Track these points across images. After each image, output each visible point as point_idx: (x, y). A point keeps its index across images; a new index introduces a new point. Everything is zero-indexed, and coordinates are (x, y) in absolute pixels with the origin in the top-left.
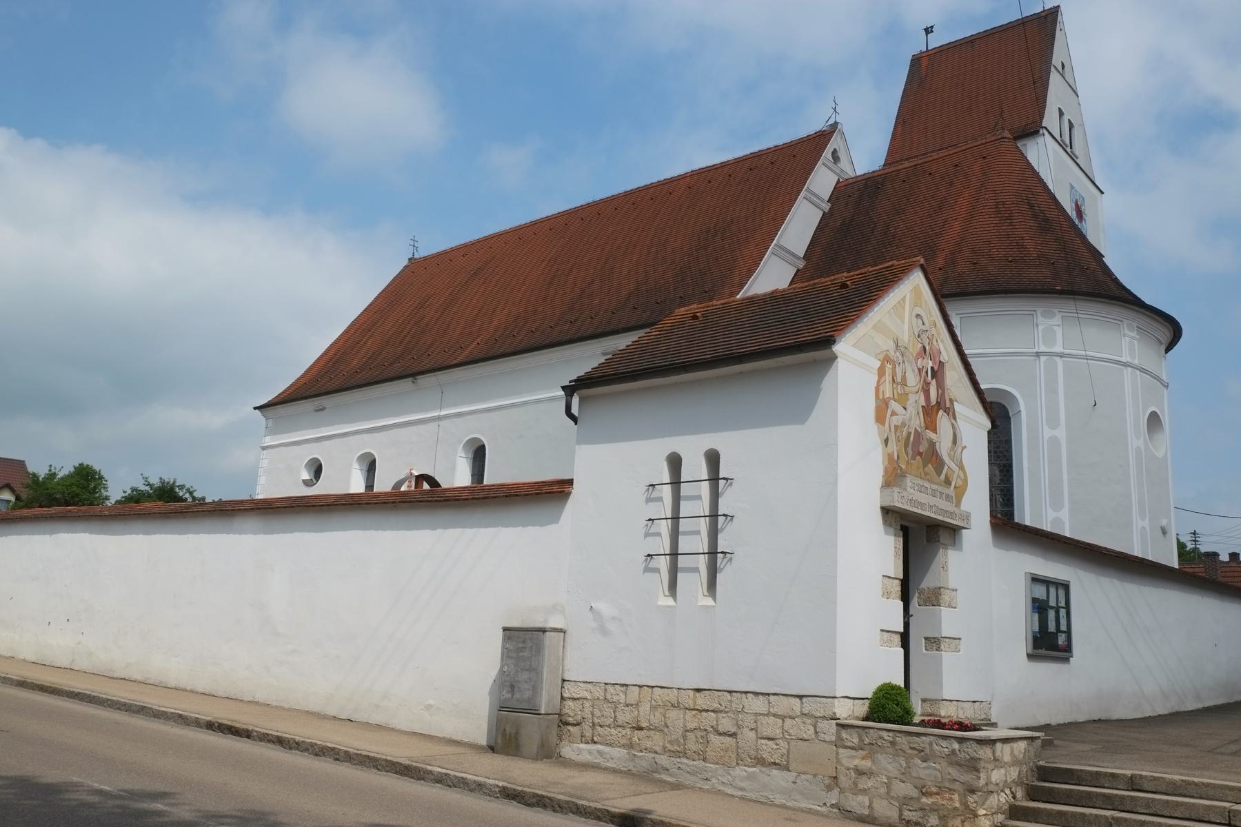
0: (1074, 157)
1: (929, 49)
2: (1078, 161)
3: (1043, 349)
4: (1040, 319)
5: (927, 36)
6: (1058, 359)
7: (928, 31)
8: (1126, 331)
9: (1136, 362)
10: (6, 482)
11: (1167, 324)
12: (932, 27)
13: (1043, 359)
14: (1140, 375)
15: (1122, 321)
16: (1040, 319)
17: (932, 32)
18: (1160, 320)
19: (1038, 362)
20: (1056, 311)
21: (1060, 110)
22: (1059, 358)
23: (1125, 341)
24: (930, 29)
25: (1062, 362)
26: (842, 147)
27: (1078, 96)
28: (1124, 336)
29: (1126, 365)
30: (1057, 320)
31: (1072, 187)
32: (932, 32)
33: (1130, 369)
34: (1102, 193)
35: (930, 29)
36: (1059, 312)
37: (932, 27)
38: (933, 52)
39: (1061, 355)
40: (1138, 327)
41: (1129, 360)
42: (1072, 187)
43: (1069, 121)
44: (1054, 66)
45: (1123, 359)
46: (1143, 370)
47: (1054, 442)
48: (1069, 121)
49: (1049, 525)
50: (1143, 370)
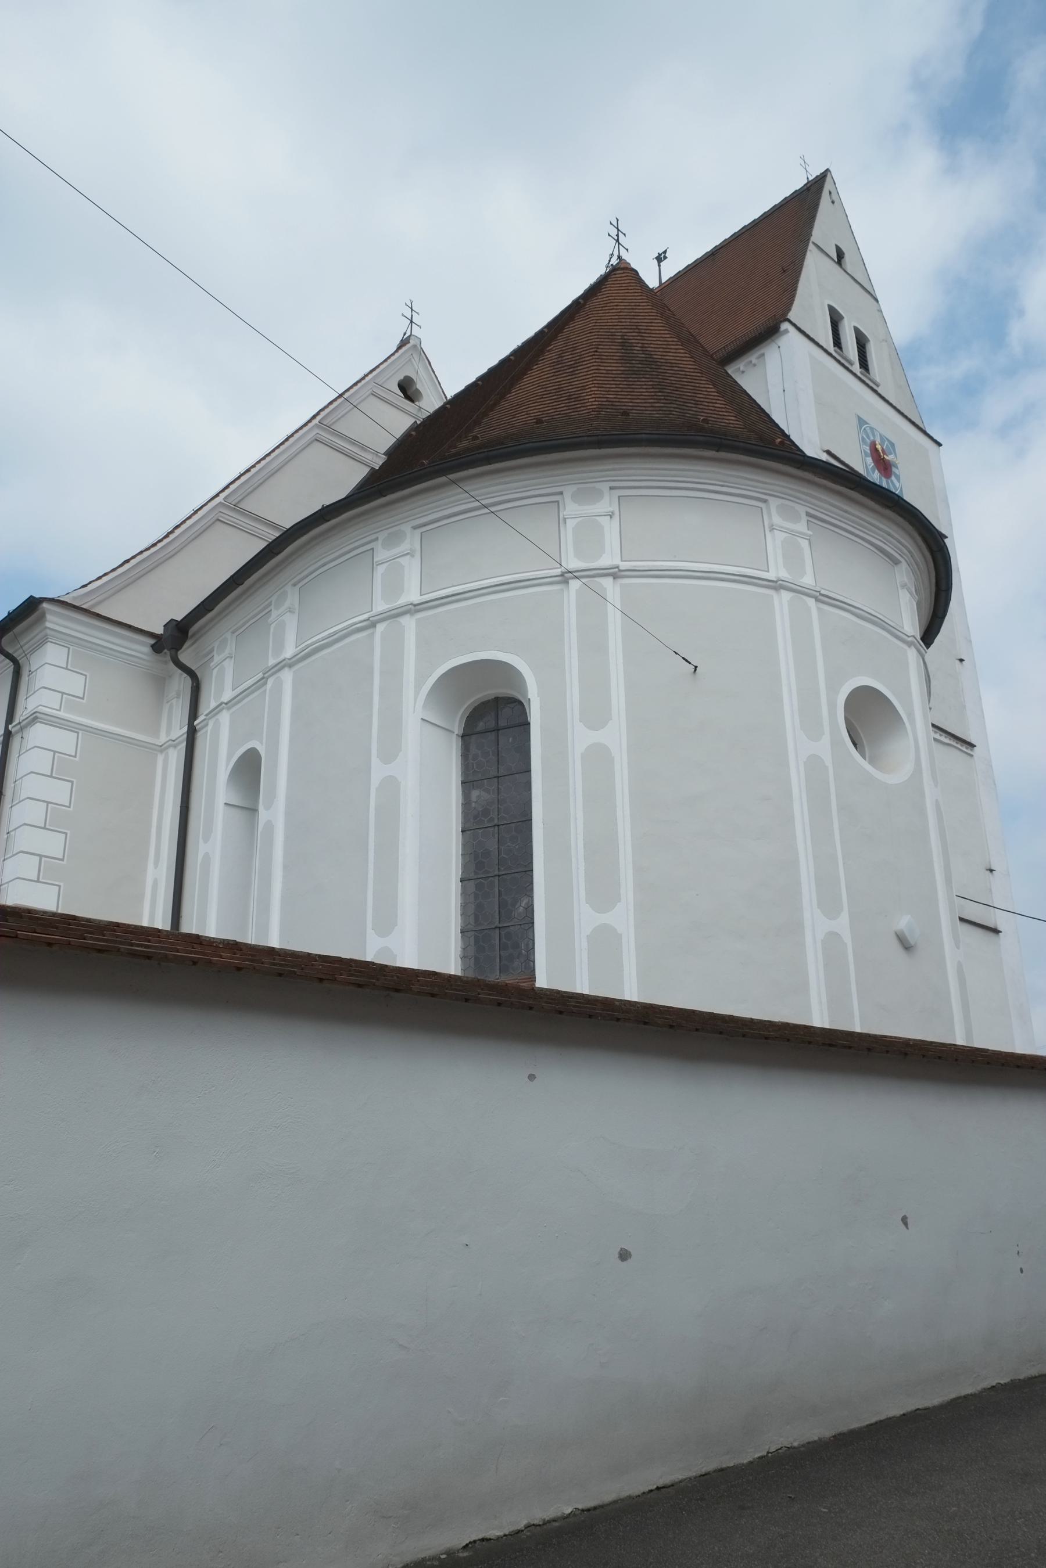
0: (847, 364)
1: (663, 281)
2: (880, 390)
3: (573, 563)
4: (571, 508)
5: (659, 266)
6: (607, 582)
7: (660, 258)
8: (777, 519)
9: (808, 580)
10: (901, 1223)
11: (888, 512)
12: (665, 252)
13: (575, 585)
14: (819, 609)
15: (765, 501)
16: (571, 508)
17: (665, 258)
18: (872, 504)
19: (565, 593)
20: (604, 487)
21: (832, 311)
22: (610, 579)
23: (775, 543)
24: (663, 255)
25: (618, 589)
26: (422, 372)
27: (877, 300)
28: (772, 529)
29: (777, 586)
30: (607, 503)
31: (861, 422)
32: (665, 258)
33: (786, 595)
34: (939, 444)
35: (663, 255)
36: (611, 488)
37: (665, 252)
38: (667, 283)
39: (615, 574)
40: (808, 514)
41: (784, 574)
42: (861, 422)
43: (857, 332)
44: (814, 243)
45: (771, 575)
46: (821, 598)
47: (600, 754)
48: (857, 332)
49: (857, 1020)
50: (821, 598)
